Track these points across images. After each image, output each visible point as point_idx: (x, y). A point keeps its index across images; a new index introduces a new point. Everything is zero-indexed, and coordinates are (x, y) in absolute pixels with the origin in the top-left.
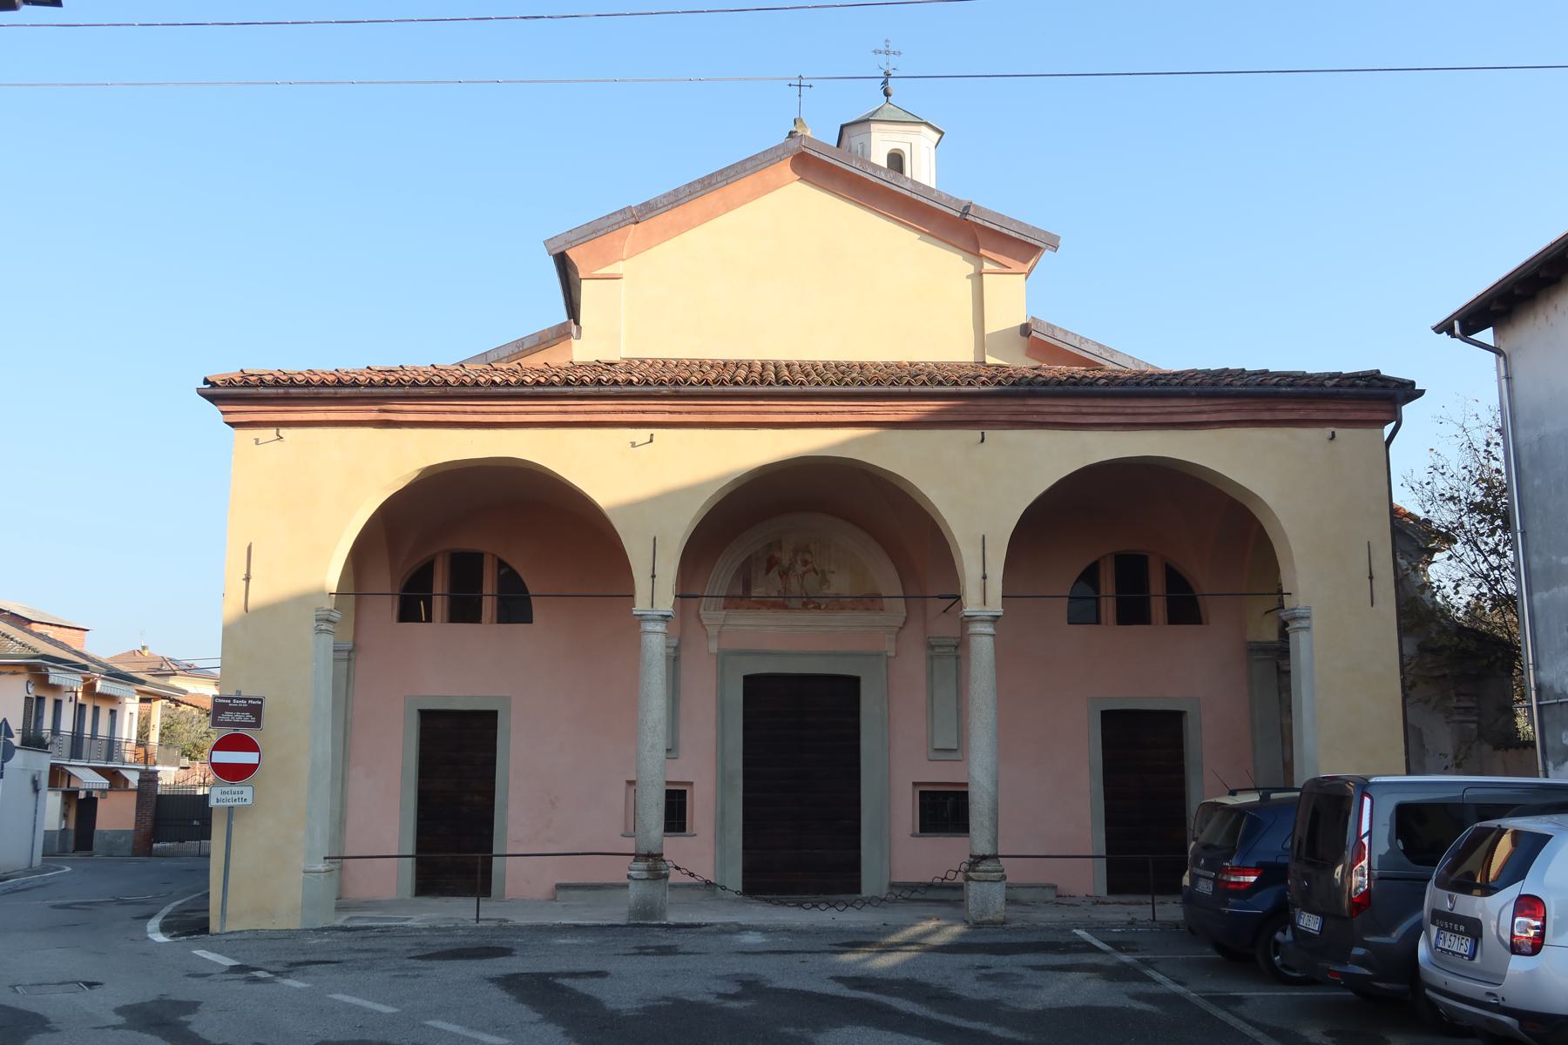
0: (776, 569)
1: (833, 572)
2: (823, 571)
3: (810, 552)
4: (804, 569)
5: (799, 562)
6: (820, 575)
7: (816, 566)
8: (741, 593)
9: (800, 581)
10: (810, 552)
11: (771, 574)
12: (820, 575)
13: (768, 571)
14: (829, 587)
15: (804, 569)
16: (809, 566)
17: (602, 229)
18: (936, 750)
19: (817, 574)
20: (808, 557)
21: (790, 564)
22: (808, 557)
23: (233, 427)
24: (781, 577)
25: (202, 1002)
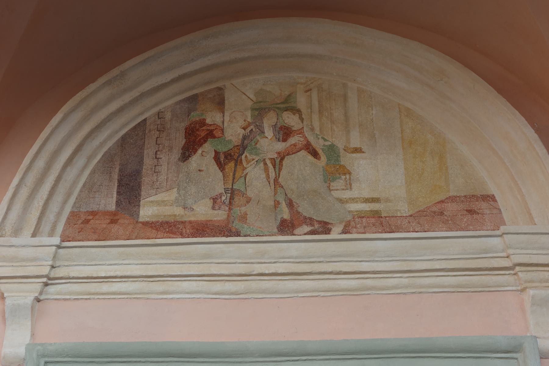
0: (208, 148)
1: (357, 150)
2: (332, 150)
3: (296, 111)
4: (281, 146)
5: (269, 133)
6: (323, 158)
7: (311, 139)
8: (112, 207)
9: (272, 174)
10: (296, 111)
11: (195, 160)
12: (323, 158)
13: (186, 155)
14: (349, 186)
15: (281, 146)
16: (293, 140)
17: (299, 137)
18: (517, 359)
19: (315, 154)
20: (291, 120)
21: (244, 138)
22: (291, 120)
23: (287, 111)
24: (221, 166)
25: (214, 150)
